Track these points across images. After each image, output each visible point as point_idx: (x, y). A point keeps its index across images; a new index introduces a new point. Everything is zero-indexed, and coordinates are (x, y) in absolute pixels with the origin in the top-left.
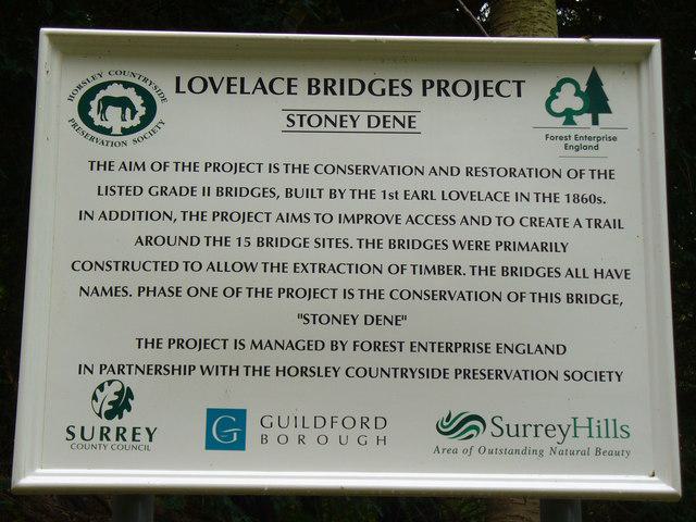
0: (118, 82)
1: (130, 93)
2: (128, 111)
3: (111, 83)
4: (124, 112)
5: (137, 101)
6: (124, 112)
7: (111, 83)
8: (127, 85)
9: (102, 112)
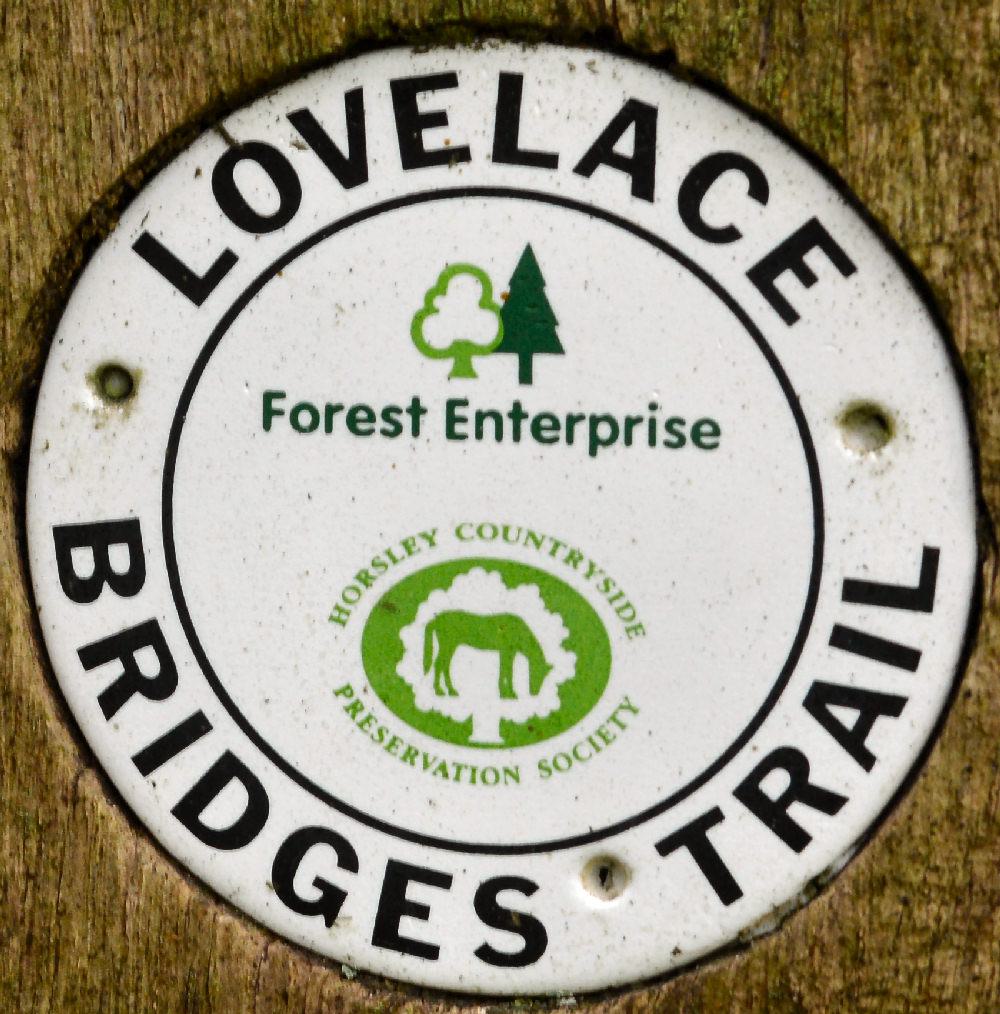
0: (489, 565)
1: (526, 602)
2: (521, 665)
3: (463, 566)
4: (506, 670)
5: (549, 630)
6: (506, 670)
7: (463, 566)
8: (514, 574)
9: (439, 665)
